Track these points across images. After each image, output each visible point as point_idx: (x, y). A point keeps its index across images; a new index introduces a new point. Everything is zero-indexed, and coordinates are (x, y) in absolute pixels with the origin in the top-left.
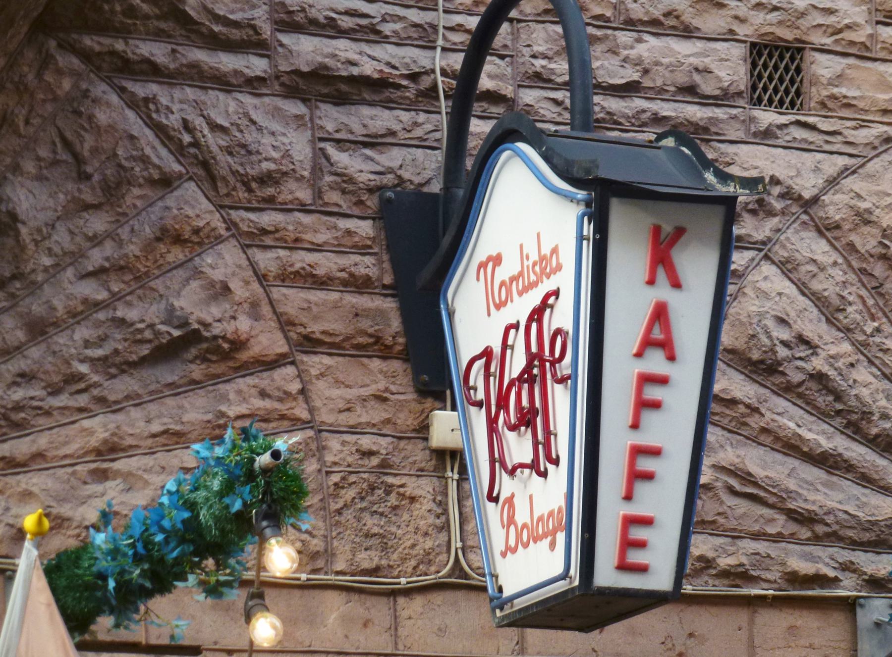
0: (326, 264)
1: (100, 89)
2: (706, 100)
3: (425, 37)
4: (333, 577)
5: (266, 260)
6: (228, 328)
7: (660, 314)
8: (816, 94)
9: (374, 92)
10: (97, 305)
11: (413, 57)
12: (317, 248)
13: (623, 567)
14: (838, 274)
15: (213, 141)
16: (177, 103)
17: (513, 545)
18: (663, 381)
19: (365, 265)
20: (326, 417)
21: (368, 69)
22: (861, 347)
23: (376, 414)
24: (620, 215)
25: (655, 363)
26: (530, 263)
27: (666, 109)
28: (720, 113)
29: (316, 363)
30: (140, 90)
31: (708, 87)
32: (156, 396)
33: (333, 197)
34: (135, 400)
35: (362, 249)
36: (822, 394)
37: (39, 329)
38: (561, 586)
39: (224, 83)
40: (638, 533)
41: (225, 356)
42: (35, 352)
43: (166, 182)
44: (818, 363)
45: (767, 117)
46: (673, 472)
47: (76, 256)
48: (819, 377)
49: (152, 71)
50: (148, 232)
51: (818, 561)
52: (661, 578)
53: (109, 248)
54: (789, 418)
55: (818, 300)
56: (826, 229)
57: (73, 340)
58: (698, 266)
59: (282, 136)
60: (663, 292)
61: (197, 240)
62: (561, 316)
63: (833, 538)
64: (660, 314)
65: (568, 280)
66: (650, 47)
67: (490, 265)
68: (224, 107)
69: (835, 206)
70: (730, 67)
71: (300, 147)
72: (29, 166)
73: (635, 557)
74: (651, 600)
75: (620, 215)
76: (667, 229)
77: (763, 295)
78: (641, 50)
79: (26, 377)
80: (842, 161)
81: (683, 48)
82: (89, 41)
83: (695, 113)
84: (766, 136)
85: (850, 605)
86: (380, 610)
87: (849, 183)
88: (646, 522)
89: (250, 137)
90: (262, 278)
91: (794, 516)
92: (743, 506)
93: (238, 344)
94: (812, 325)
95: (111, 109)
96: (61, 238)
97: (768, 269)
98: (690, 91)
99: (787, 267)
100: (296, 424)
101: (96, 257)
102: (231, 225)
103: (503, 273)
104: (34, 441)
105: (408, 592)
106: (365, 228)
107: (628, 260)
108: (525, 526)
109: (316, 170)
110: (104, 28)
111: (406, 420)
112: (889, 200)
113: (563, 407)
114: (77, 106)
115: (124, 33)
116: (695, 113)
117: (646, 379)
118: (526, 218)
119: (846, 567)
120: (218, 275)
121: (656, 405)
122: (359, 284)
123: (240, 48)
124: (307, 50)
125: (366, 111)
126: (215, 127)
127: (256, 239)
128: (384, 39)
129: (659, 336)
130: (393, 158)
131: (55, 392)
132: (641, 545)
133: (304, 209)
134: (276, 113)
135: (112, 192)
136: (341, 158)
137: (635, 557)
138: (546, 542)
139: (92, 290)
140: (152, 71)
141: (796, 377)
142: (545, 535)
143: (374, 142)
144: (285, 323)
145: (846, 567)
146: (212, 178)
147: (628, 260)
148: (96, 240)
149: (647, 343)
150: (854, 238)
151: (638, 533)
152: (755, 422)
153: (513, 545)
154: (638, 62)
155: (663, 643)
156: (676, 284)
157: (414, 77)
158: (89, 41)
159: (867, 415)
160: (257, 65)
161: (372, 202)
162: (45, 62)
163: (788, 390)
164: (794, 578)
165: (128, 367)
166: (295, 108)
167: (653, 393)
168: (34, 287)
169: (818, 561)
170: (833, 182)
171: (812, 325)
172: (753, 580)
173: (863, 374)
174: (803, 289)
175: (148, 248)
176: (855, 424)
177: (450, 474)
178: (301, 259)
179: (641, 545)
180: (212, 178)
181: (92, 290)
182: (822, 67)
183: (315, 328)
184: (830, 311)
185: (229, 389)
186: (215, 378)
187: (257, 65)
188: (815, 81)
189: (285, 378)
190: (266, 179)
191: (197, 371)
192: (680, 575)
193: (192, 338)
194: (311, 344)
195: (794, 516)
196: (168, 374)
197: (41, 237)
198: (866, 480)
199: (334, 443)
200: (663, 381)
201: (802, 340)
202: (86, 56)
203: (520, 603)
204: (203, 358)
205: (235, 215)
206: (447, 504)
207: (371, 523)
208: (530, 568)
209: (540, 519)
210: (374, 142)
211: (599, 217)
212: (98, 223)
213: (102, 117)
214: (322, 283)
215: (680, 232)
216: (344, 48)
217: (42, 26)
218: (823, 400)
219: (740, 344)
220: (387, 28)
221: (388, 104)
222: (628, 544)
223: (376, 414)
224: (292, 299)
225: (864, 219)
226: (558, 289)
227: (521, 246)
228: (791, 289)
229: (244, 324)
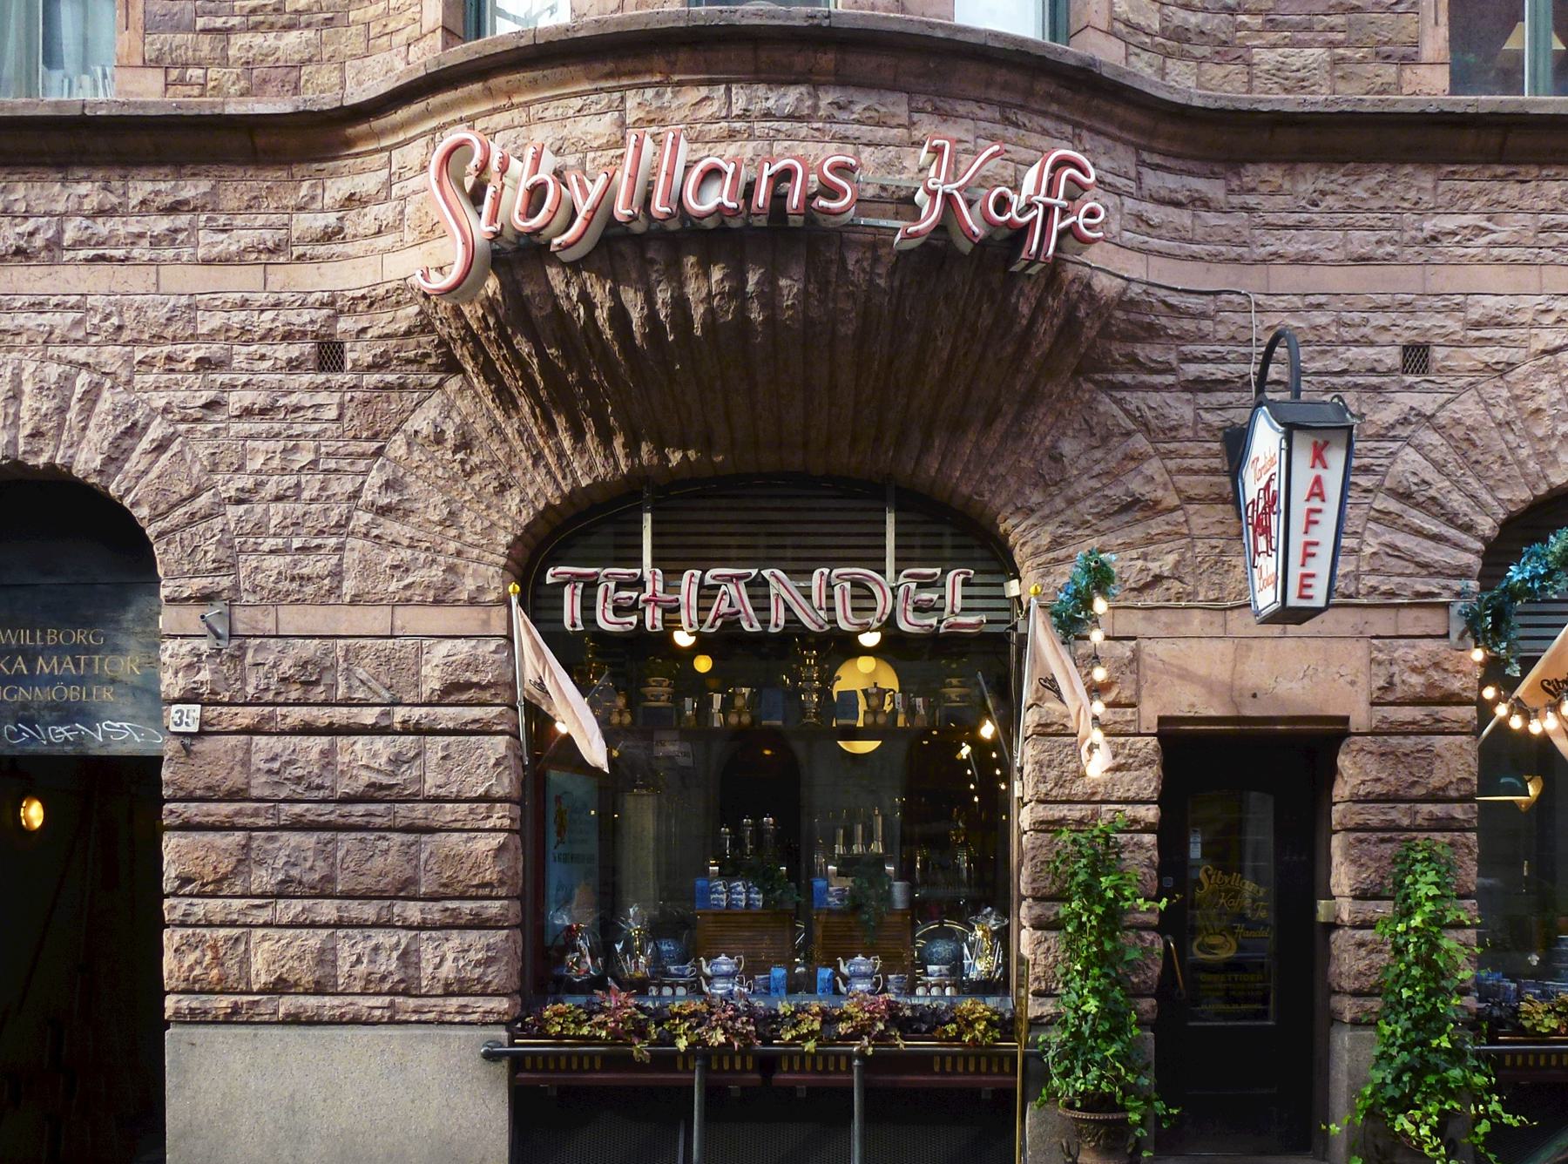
0: (1198, 463)
1: (1103, 397)
2: (1384, 374)
3: (1247, 358)
5: (1171, 464)
6: (1152, 496)
7: (1318, 481)
8: (1434, 366)
10: (1097, 490)
11: (1241, 368)
12: (1194, 457)
13: (1301, 597)
14: (1444, 449)
15: (1149, 414)
16: (1134, 399)
18: (1319, 511)
19: (1215, 463)
20: (1196, 532)
21: (1220, 376)
22: (1455, 483)
23: (1219, 529)
24: (1297, 436)
25: (1316, 503)
27: (1360, 380)
28: (1386, 379)
29: (1192, 508)
30: (1118, 395)
31: (1381, 368)
32: (1121, 528)
33: (1203, 433)
34: (1111, 530)
35: (1215, 456)
36: (1434, 506)
37: (1071, 502)
38: (1275, 606)
39: (1156, 388)
40: (1308, 581)
41: (1152, 508)
42: (1069, 512)
43: (1128, 434)
44: (1432, 492)
45: (1410, 379)
46: (1325, 552)
47: (1087, 470)
48: (1433, 499)
49: (1124, 386)
50: (1120, 456)
51: (1433, 585)
52: (1319, 601)
53: (1102, 465)
54: (1417, 518)
55: (1434, 462)
56: (1439, 429)
57: (1082, 507)
58: (1336, 458)
59: (1180, 409)
60: (1319, 471)
61: (1142, 458)
62: (1274, 486)
63: (1439, 574)
64: (1318, 481)
65: (1278, 469)
66: (1353, 352)
68: (1155, 399)
69: (1443, 418)
70: (1392, 357)
71: (1188, 412)
72: (1070, 433)
73: (1307, 592)
74: (1315, 612)
75: (1297, 436)
76: (1321, 442)
77: (1406, 462)
78: (1349, 355)
79: (1065, 523)
80: (1447, 396)
81: (1370, 352)
82: (1097, 377)
83: (1375, 380)
84: (1410, 388)
85: (1446, 606)
86: (1218, 617)
87: (1450, 406)
89: (1166, 411)
90: (1169, 472)
91: (1418, 564)
92: (1394, 561)
93: (1157, 502)
94: (1430, 474)
95: (1106, 404)
96: (1082, 462)
97: (1409, 449)
98: (1372, 370)
99: (1418, 448)
100: (1183, 536)
101: (1097, 469)
102: (1156, 450)
103: (1260, 465)
104: (474, 647)
105: (1231, 609)
106: (1216, 446)
107: (1302, 459)
109: (1196, 423)
110: (1104, 370)
111: (1233, 531)
113: (1276, 523)
114: (1090, 406)
115: (1113, 371)
116: (1375, 380)
118: (1266, 440)
119: (1445, 588)
120: (1149, 473)
121: (1316, 522)
122: (1213, 472)
124: (1192, 370)
125: (1219, 394)
126: (1150, 408)
127: (1168, 455)
128: (1229, 362)
129: (1317, 490)
130: (1230, 414)
131: (1077, 528)
132: (1310, 586)
133: (1189, 440)
134: (1178, 399)
135: (1105, 440)
136: (1206, 416)
137: (1307, 592)
139: (1095, 484)
140: (1124, 386)
141: (1421, 499)
143: (1222, 408)
144: (1179, 491)
145: (1445, 588)
146: (1149, 430)
147: (1302, 459)
148: (1097, 462)
149: (1312, 495)
150: (1453, 432)
151: (1308, 581)
152: (1400, 521)
154: (1346, 360)
157: (1241, 377)
158: (1097, 377)
159: (1456, 515)
160: (1170, 379)
161: (1220, 434)
162: (1078, 387)
163: (1417, 505)
164: (1418, 594)
165: (1108, 516)
166: (1188, 396)
168: (1070, 484)
169: (1433, 585)
170: (1442, 406)
171: (1430, 474)
172: (1399, 595)
173: (1455, 496)
174: (1426, 457)
175: (1119, 464)
176: (1451, 519)
178: (1187, 462)
179: (1310, 586)
180: (1149, 430)
181: (1095, 484)
182: (1438, 353)
183: (1191, 493)
184: (1439, 467)
185: (1152, 522)
186: (1147, 518)
187: (1170, 379)
188: (1434, 360)
189: (1178, 516)
190: (1172, 429)
191: (1139, 515)
192: (1329, 596)
193: (1136, 501)
194: (1190, 500)
195: (1418, 564)
196: (1126, 518)
197: (1073, 462)
198: (1456, 545)
199: (1199, 543)
200: (1319, 511)
201: (1424, 482)
202: (1096, 383)
203: (1264, 613)
204: (1141, 509)
205: (1159, 445)
207: (1215, 579)
208: (1266, 599)
210: (1222, 408)
211: (1289, 438)
212: (1098, 454)
213: (1101, 409)
214: (1197, 472)
215: (1326, 443)
216: (1209, 367)
217: (1077, 372)
218: (1435, 509)
219: (1394, 486)
220: (1229, 357)
221: (1229, 390)
222: (1303, 586)
223: (1219, 529)
224: (1182, 480)
225: (1458, 422)
228: (1418, 457)
229: (1160, 494)
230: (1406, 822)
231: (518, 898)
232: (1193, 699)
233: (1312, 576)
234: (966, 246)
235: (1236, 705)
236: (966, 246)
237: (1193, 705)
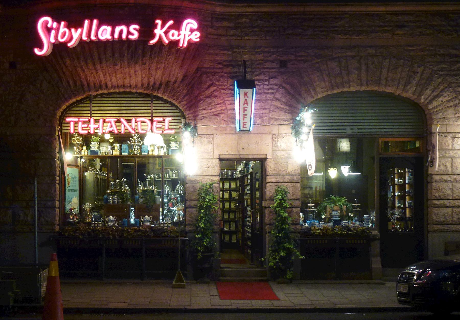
4: (375, 165)
7: (246, 100)
13: (244, 127)
18: (247, 107)
25: (246, 105)
40: (245, 124)
60: (246, 98)
64: (246, 100)
73: (245, 126)
112: (458, 65)
117: (245, 107)
123: (239, 15)
137: (245, 126)
151: (245, 124)
155: (125, 78)
167: (246, 109)
200: (247, 107)
222: (244, 125)
230: (282, 181)
231: (428, 175)
232: (228, 150)
233: (246, 122)
234: (166, 45)
235: (238, 151)
236: (166, 45)
237: (227, 151)
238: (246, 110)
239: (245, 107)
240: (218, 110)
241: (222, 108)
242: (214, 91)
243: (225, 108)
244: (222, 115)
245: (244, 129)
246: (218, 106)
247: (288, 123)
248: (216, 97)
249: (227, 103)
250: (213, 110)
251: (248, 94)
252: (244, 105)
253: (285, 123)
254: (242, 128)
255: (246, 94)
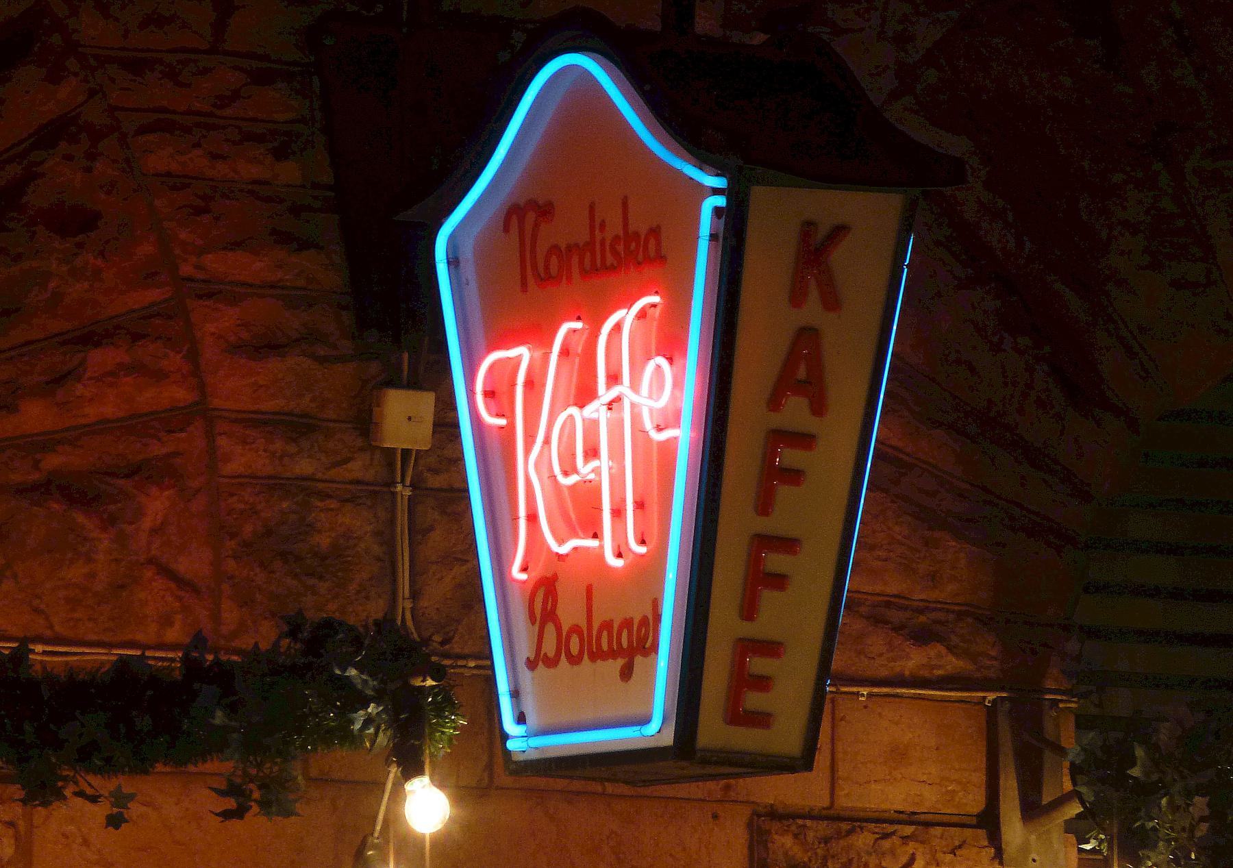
7: (806, 342)
9: (322, 501)
13: (738, 716)
17: (551, 654)
18: (805, 440)
25: (796, 413)
26: (609, 236)
40: (758, 665)
46: (810, 576)
60: (812, 312)
64: (806, 342)
67: (531, 217)
73: (754, 700)
88: (789, 545)
108: (575, 629)
117: (780, 437)
137: (754, 700)
138: (620, 662)
142: (612, 654)
153: (551, 654)
156: (832, 302)
167: (789, 457)
177: (399, 487)
179: (763, 683)
200: (805, 440)
206: (393, 537)
209: (607, 625)
222: (744, 681)
226: (659, 227)
227: (592, 209)
238: (794, 476)
239: (780, 437)
240: (92, 413)
241: (153, 397)
242: (54, 133)
243: (180, 394)
244: (157, 504)
245: (746, 739)
246: (102, 358)
247: (952, 664)
248: (74, 222)
249: (216, 324)
250: (35, 416)
251: (839, 257)
252: (775, 403)
253: (914, 660)
254: (713, 731)
255: (814, 252)
